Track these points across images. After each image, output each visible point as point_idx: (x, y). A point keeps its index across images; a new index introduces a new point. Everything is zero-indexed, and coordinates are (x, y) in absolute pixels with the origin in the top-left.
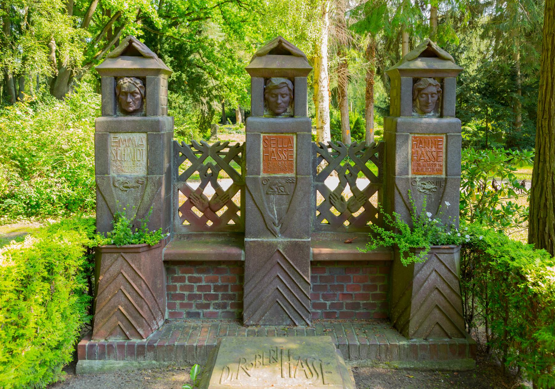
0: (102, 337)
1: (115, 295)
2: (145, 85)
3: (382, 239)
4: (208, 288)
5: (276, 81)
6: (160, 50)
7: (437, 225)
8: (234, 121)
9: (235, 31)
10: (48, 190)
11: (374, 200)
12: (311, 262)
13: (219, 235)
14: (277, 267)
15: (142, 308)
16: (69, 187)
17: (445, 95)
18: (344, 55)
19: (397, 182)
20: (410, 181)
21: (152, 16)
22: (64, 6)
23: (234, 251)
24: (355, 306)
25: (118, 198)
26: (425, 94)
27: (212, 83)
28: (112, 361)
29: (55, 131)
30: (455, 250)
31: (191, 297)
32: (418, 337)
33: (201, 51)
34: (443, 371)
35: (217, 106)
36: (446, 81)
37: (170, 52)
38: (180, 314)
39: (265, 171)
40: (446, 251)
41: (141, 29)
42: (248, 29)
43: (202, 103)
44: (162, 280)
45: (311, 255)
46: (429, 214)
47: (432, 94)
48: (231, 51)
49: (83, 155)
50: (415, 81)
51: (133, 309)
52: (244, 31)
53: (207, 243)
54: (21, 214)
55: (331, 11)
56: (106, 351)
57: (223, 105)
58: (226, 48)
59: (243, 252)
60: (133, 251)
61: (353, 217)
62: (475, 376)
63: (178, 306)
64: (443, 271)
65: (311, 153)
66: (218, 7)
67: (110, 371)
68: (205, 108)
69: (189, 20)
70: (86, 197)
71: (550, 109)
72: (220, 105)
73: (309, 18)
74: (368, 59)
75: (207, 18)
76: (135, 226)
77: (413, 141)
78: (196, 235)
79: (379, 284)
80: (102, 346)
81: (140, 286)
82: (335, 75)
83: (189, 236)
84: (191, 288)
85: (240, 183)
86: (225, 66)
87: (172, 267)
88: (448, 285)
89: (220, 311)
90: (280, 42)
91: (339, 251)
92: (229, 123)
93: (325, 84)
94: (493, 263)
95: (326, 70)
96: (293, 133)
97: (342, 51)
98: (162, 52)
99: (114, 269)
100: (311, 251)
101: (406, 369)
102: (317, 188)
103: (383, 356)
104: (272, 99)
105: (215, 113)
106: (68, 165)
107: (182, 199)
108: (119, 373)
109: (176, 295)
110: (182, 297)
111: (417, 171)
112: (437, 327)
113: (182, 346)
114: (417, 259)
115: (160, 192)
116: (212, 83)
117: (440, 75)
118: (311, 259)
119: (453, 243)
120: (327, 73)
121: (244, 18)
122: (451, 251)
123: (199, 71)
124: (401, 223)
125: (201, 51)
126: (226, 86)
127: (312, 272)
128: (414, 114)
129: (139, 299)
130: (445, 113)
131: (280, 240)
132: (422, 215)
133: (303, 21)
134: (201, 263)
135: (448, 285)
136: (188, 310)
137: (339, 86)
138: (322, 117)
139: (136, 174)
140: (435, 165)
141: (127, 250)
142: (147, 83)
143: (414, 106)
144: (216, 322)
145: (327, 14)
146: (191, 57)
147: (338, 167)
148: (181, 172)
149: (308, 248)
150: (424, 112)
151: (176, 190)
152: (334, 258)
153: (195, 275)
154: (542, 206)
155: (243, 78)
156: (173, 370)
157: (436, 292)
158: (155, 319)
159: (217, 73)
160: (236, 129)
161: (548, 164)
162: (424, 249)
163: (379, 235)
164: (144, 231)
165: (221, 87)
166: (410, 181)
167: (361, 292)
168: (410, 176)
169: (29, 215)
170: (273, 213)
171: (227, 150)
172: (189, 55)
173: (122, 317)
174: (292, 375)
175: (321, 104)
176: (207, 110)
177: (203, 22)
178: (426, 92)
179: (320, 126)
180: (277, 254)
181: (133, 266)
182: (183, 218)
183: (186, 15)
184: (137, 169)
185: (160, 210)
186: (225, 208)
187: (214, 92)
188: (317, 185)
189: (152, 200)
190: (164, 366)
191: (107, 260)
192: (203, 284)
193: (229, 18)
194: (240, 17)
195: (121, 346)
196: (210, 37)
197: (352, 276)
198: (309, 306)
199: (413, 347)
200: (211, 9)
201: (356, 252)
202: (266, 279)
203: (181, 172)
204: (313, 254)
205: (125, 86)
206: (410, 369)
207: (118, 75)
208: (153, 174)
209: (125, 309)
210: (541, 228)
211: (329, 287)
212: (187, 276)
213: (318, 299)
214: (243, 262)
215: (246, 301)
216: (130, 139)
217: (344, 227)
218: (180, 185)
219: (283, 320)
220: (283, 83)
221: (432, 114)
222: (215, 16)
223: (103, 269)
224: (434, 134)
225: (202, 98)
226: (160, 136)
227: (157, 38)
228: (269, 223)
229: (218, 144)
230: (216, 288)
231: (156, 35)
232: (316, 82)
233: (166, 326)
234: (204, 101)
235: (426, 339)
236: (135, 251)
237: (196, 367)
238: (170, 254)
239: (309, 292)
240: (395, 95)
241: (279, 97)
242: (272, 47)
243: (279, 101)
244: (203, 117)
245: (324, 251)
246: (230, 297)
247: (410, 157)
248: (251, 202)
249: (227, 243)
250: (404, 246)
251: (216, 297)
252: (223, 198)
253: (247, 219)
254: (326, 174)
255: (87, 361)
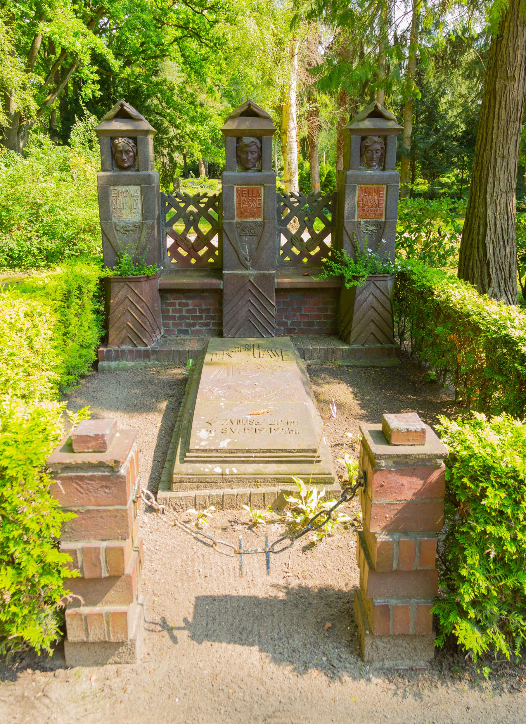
0: (115, 345)
1: (123, 314)
2: (136, 144)
3: (332, 271)
4: (194, 311)
5: (247, 140)
6: (114, 94)
7: (376, 259)
8: (198, 175)
9: (195, 72)
10: (28, 243)
11: (328, 241)
12: (276, 289)
13: (201, 271)
14: (249, 294)
15: (145, 323)
16: (47, 240)
17: (387, 151)
18: (316, 101)
19: (345, 225)
20: (356, 224)
21: (107, 57)
22: (14, 49)
23: (214, 282)
24: (311, 324)
25: (119, 239)
26: (371, 150)
27: (173, 132)
28: (125, 362)
29: (28, 186)
30: (389, 278)
31: (181, 318)
32: (357, 344)
33: (159, 95)
34: (374, 367)
35: (178, 158)
36: (388, 139)
37: (125, 96)
38: (173, 331)
39: (238, 216)
40: (382, 279)
41: (96, 73)
42: (210, 70)
43: (163, 155)
44: (158, 305)
45: (276, 284)
46: (370, 250)
47: (377, 150)
48: (192, 95)
49: (58, 209)
50: (363, 139)
51: (138, 324)
52: (206, 72)
53: (192, 276)
54: (4, 266)
55: (300, 53)
56: (119, 355)
57: (185, 156)
58: (186, 92)
59: (222, 282)
60: (136, 280)
61: (310, 255)
62: (398, 370)
63: (171, 325)
64: (378, 294)
65: (276, 202)
66: (175, 43)
67: (124, 369)
68: (166, 160)
69: (144, 59)
70: (64, 250)
71: (482, 161)
72: (181, 157)
73: (277, 62)
74: (340, 105)
75: (164, 56)
76: (136, 261)
77: (359, 190)
78: (183, 271)
79: (330, 307)
80: (117, 351)
81: (142, 307)
82: (305, 124)
83: (176, 272)
84: (181, 311)
85: (218, 228)
86: (187, 113)
87: (165, 295)
88: (382, 305)
89: (204, 328)
90: (250, 105)
91: (299, 281)
92: (192, 177)
93: (294, 135)
94: (415, 286)
95: (295, 119)
96: (261, 185)
97: (312, 97)
98: (117, 96)
99: (121, 295)
100: (276, 281)
101: (347, 366)
102: (281, 231)
103: (330, 357)
104: (243, 156)
105: (178, 165)
106: (45, 219)
107: (170, 241)
108: (130, 370)
109: (169, 316)
110: (173, 318)
111: (361, 216)
112: (372, 336)
113: (178, 351)
114: (359, 284)
115: (154, 234)
116: (173, 132)
117: (384, 134)
118: (276, 287)
119: (388, 273)
120: (295, 122)
121: (206, 56)
122: (385, 279)
123: (157, 118)
124: (347, 258)
125: (159, 95)
126: (188, 135)
127: (277, 298)
128: (362, 167)
129: (143, 317)
130: (387, 167)
131: (251, 272)
132: (364, 251)
133: (270, 64)
134: (189, 291)
135: (382, 305)
136: (179, 328)
137: (308, 136)
138: (289, 169)
139: (133, 220)
140: (377, 210)
141: (131, 280)
142: (138, 142)
143: (361, 161)
144: (202, 336)
145: (296, 56)
146: (149, 101)
147: (298, 214)
148: (168, 218)
149: (273, 278)
150: (370, 166)
151: (165, 234)
152: (294, 286)
153: (183, 301)
154: (469, 245)
155: (206, 127)
156: (171, 368)
157: (372, 310)
158: (155, 333)
159: (178, 121)
160: (200, 183)
161: (476, 210)
162: (363, 277)
163: (330, 267)
164: (143, 266)
165: (183, 137)
166: (356, 224)
167: (316, 313)
168: (356, 220)
169: (13, 267)
170: (246, 251)
171: (205, 200)
172: (145, 100)
173: (130, 330)
174: (261, 356)
175: (290, 156)
176: (168, 163)
177: (159, 60)
178: (371, 148)
179: (288, 179)
180: (249, 283)
181: (136, 292)
182: (171, 257)
183: (140, 53)
184: (134, 216)
185: (154, 249)
186: (206, 249)
187: (175, 143)
188: (281, 229)
189: (147, 241)
190: (164, 365)
191: (115, 288)
192: (191, 308)
193: (189, 56)
194: (201, 55)
195: (131, 351)
196: (169, 78)
197: (308, 300)
198: (274, 323)
199: (353, 350)
200: (169, 45)
201: (311, 281)
202: (240, 303)
203: (168, 218)
204: (278, 283)
205: (120, 145)
206: (350, 366)
207: (113, 135)
208: (147, 219)
209: (132, 324)
210: (466, 263)
211: (290, 310)
212: (177, 301)
213: (282, 319)
214: (221, 290)
215: (225, 320)
216: (126, 191)
217: (303, 263)
218: (168, 230)
219: (254, 334)
220: (252, 142)
221: (376, 167)
222: (173, 54)
223: (113, 294)
224: (377, 184)
225: (162, 149)
226: (152, 188)
227: (109, 80)
228: (242, 259)
229: (198, 195)
230: (201, 311)
231: (108, 76)
232: (285, 133)
233: (163, 339)
234: (166, 151)
235: (363, 345)
236: (137, 280)
237: (191, 361)
238: (164, 284)
239: (274, 313)
240: (346, 151)
241: (249, 154)
242: (242, 110)
243: (249, 158)
244: (164, 170)
245: (286, 281)
246: (212, 318)
247: (356, 204)
248: (228, 242)
249: (208, 276)
250: (348, 274)
251: (201, 318)
252: (203, 240)
253: (224, 256)
254: (288, 219)
255: (106, 362)
